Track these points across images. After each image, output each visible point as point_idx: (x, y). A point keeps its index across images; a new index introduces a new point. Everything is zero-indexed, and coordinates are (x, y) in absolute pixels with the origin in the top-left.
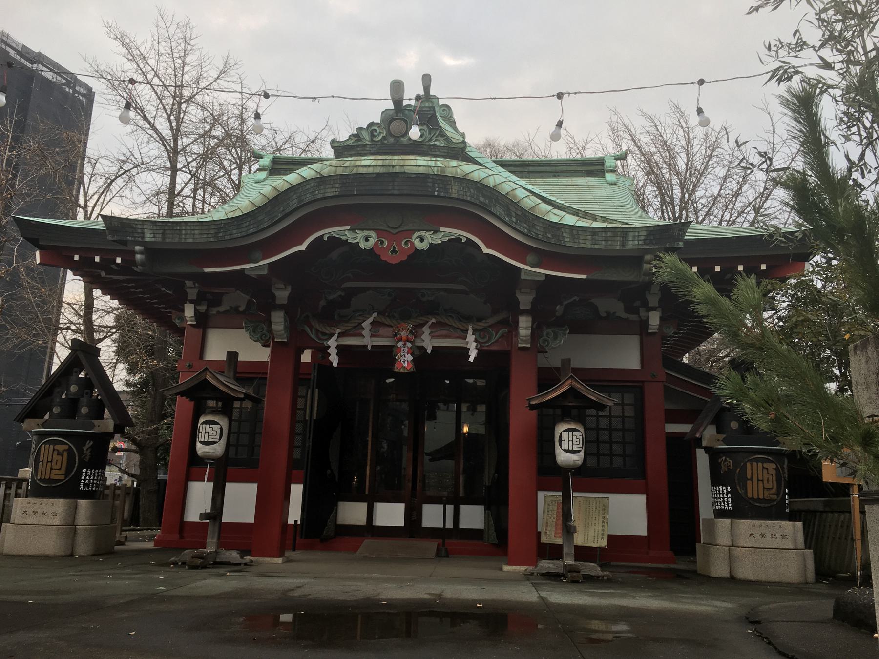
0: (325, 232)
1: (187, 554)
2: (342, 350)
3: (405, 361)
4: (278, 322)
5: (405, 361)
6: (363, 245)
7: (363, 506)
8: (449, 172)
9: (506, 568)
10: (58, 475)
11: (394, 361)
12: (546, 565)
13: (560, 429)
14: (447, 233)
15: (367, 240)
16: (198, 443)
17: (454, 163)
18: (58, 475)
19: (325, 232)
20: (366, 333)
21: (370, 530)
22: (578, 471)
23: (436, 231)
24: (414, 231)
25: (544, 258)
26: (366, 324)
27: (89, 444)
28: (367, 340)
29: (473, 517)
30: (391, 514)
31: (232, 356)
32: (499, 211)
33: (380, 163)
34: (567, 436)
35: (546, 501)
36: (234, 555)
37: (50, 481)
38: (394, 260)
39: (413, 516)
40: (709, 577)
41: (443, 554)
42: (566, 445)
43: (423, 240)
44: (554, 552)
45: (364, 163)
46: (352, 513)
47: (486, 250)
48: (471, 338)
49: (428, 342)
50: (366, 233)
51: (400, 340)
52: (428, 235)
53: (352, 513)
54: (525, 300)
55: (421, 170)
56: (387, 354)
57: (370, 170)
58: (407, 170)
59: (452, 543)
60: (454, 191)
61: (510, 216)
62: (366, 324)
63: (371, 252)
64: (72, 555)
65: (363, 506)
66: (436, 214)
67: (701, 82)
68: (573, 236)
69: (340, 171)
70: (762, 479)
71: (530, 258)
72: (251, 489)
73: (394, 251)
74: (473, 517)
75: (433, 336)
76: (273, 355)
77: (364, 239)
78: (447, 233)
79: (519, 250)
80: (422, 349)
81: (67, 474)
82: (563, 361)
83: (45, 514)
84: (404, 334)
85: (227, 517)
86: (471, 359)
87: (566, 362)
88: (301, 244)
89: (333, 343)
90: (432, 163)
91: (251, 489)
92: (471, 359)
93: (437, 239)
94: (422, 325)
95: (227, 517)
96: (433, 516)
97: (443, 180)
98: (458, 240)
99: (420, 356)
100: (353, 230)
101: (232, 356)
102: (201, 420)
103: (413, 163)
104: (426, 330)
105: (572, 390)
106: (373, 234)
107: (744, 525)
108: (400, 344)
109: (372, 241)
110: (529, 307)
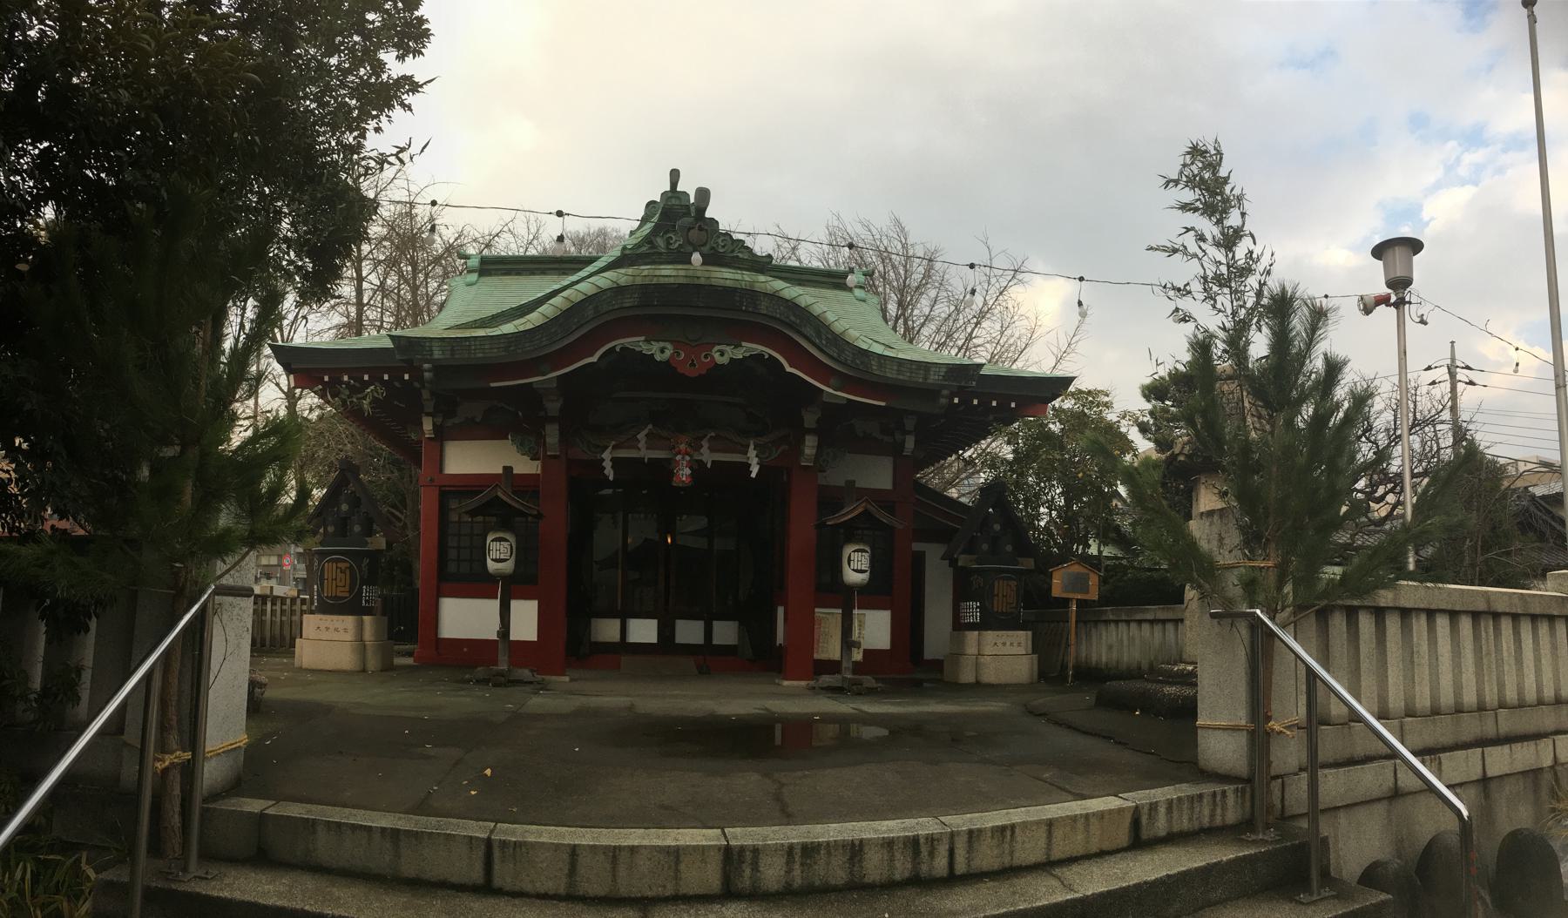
0: (617, 343)
1: (480, 672)
2: (616, 462)
3: (684, 474)
4: (552, 435)
5: (684, 474)
6: (658, 357)
7: (617, 623)
8: (758, 287)
9: (786, 683)
10: (343, 592)
11: (671, 474)
12: (826, 679)
13: (848, 550)
14: (750, 348)
15: (662, 351)
16: (489, 561)
17: (762, 278)
18: (343, 592)
19: (617, 343)
20: (642, 445)
21: (625, 647)
22: (862, 589)
23: (738, 346)
24: (714, 345)
25: (847, 383)
26: (641, 436)
27: (366, 561)
28: (644, 453)
29: (726, 633)
30: (644, 631)
31: (508, 469)
32: (809, 331)
33: (682, 273)
34: (855, 556)
35: (829, 619)
36: (525, 673)
37: (336, 598)
38: (692, 373)
39: (666, 632)
40: (957, 684)
41: (704, 671)
42: (854, 565)
43: (724, 354)
44: (832, 667)
45: (664, 273)
46: (608, 630)
47: (789, 369)
48: (752, 453)
49: (708, 457)
50: (662, 344)
51: (679, 453)
52: (728, 349)
53: (608, 630)
54: (810, 419)
55: (728, 283)
56: (663, 469)
57: (672, 280)
58: (714, 282)
59: (709, 661)
60: (764, 307)
61: (820, 337)
62: (641, 436)
63: (667, 363)
64: (364, 671)
65: (617, 623)
66: (738, 330)
67: (1081, 279)
68: (880, 366)
69: (639, 281)
70: (1005, 594)
71: (832, 381)
72: (533, 606)
73: (693, 364)
74: (726, 633)
75: (712, 450)
76: (543, 468)
77: (660, 351)
78: (750, 348)
79: (824, 372)
80: (700, 462)
81: (350, 592)
82: (848, 482)
83: (336, 630)
84: (683, 447)
85: (515, 636)
86: (753, 475)
87: (851, 483)
88: (592, 355)
89: (607, 455)
90: (738, 277)
91: (533, 606)
92: (753, 475)
93: (739, 354)
94: (701, 439)
95: (515, 636)
96: (689, 632)
97: (752, 294)
98: (760, 356)
99: (698, 468)
100: (647, 341)
101: (508, 469)
102: (489, 539)
103: (718, 275)
104: (705, 443)
105: (866, 513)
106: (668, 345)
107: (990, 636)
108: (678, 457)
109: (668, 353)
110: (814, 426)
